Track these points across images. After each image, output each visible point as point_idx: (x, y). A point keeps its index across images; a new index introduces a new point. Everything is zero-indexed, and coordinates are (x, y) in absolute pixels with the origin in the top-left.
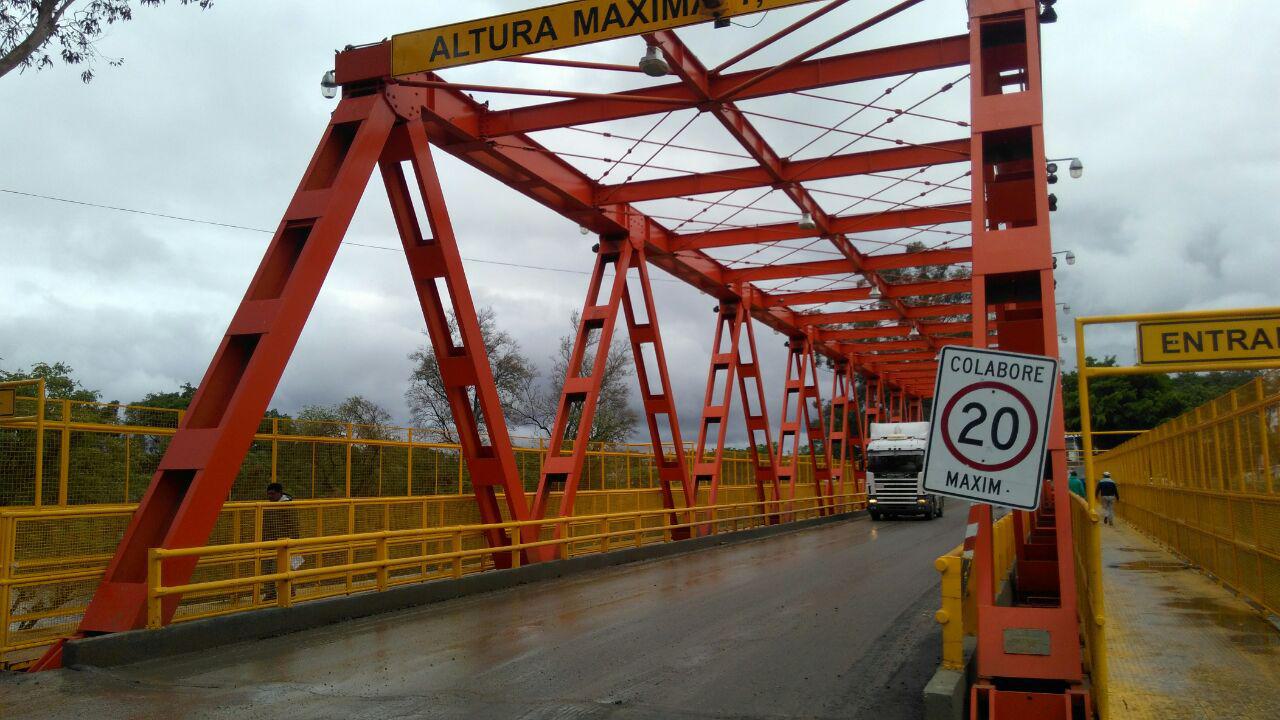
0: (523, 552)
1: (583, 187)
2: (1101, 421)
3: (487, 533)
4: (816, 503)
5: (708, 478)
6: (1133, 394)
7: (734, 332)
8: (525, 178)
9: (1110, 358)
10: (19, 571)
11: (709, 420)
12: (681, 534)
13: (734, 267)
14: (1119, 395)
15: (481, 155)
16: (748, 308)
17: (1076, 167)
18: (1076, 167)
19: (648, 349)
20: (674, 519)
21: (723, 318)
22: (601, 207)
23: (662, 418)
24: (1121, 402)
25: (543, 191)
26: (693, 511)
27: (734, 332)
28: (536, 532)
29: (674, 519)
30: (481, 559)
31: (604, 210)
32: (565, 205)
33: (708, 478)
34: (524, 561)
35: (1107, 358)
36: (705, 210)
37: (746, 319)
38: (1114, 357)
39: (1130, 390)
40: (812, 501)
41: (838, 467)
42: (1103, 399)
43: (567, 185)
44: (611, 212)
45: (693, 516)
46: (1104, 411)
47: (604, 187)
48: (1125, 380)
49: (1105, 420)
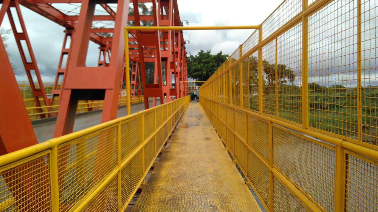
0: (49, 114)
1: (61, 15)
2: (205, 74)
3: (38, 109)
4: (87, 105)
5: (58, 95)
6: (216, 64)
7: (104, 55)
8: (45, 13)
9: (209, 51)
10: (232, 84)
11: (59, 74)
12: (90, 109)
13: (69, 14)
14: (211, 64)
15: (34, 8)
16: (108, 48)
17: (189, 42)
18: (189, 42)
19: (23, 43)
20: (88, 105)
21: (67, 35)
22: (37, 4)
23: (32, 72)
24: (212, 67)
25: (50, 17)
26: (94, 103)
27: (104, 55)
28: (51, 109)
29: (88, 105)
30: (38, 116)
31: (67, 22)
32: (56, 20)
33: (58, 95)
34: (49, 116)
35: (208, 51)
36: (76, 9)
37: (107, 51)
38: (210, 51)
39: (215, 63)
40: (85, 105)
41: (133, 90)
42: (206, 65)
43: (56, 14)
44: (69, 23)
45: (93, 105)
46: (206, 70)
47: (67, 16)
48: (214, 59)
49: (206, 74)
